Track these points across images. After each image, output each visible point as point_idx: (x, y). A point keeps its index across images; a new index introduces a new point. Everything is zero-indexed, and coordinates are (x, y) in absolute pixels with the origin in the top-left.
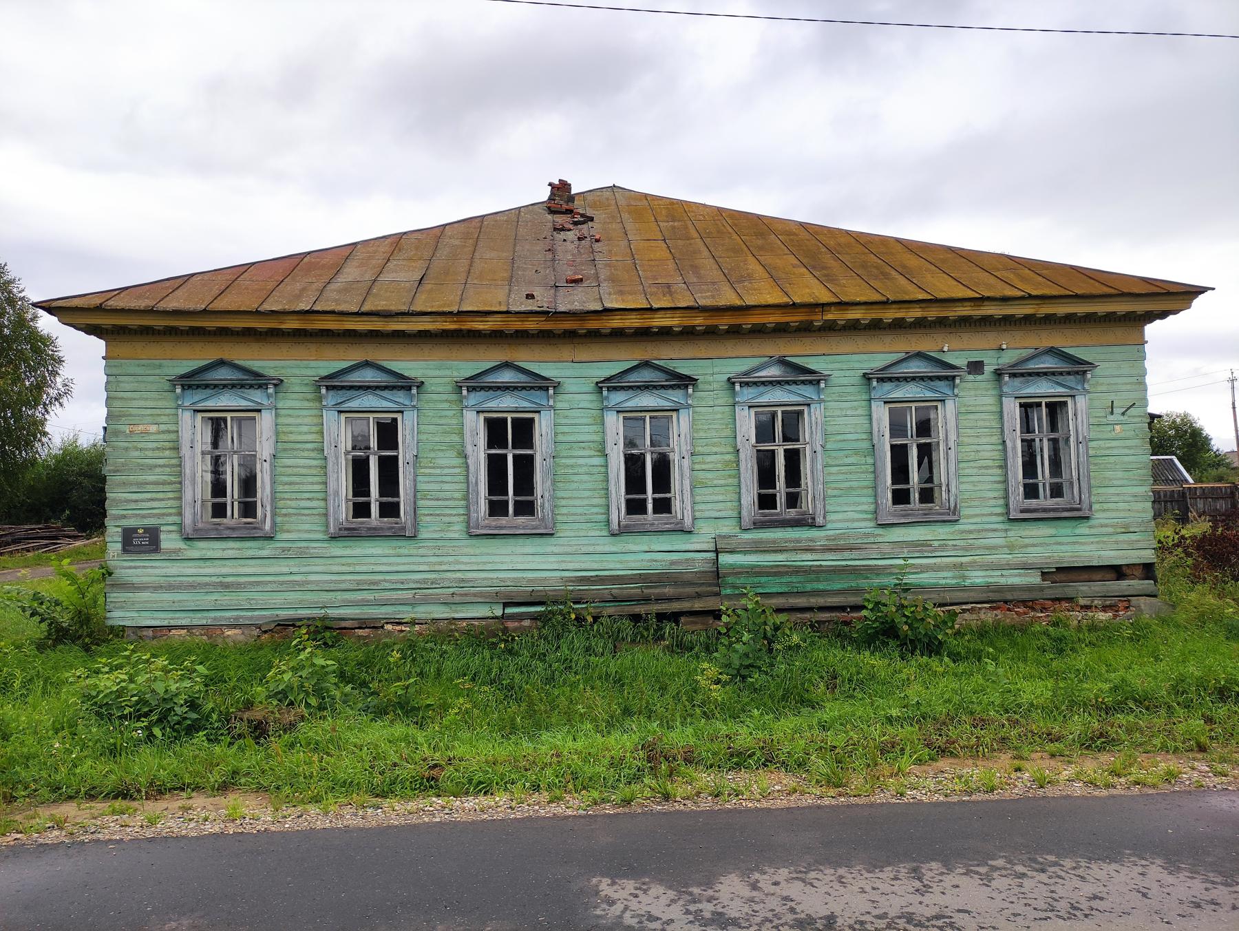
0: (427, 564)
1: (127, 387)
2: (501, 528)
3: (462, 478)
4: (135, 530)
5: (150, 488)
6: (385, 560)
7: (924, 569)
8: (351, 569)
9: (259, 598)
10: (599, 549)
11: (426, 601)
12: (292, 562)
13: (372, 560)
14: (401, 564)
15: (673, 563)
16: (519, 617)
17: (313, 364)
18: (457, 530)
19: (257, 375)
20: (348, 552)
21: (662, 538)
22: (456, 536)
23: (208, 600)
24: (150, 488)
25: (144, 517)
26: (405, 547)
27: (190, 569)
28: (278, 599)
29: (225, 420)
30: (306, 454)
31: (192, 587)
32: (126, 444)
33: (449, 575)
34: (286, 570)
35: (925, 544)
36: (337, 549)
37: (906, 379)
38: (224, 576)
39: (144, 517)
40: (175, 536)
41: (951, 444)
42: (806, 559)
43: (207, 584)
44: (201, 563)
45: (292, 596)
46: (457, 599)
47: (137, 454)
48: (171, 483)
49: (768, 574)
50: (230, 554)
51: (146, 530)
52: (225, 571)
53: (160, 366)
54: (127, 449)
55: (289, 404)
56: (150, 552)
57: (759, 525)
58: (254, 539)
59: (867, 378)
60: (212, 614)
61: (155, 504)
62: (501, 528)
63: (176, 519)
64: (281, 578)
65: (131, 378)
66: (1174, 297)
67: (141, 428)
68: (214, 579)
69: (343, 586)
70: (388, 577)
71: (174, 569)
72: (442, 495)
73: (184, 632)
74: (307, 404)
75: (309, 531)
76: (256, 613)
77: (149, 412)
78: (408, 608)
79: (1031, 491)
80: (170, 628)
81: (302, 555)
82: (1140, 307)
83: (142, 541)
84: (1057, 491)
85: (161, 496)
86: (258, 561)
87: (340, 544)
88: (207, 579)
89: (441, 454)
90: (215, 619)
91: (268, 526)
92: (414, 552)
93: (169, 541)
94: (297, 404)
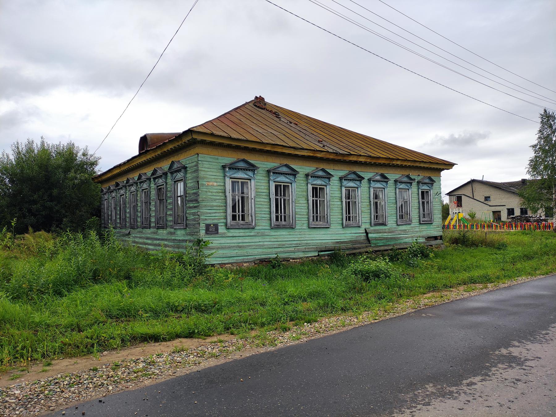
0: (297, 238)
1: (207, 166)
2: (317, 225)
3: (306, 208)
4: (209, 225)
5: (215, 208)
6: (286, 236)
7: (407, 238)
8: (277, 240)
9: (250, 251)
10: (340, 232)
11: (299, 251)
12: (260, 238)
13: (282, 237)
14: (290, 238)
15: (357, 237)
16: (324, 255)
17: (266, 163)
18: (305, 226)
19: (253, 165)
20: (276, 234)
21: (354, 229)
22: (305, 228)
23: (234, 252)
24: (215, 208)
25: (213, 219)
26: (292, 232)
27: (228, 241)
28: (256, 251)
29: (281, 185)
30: (264, 197)
31: (230, 247)
32: (206, 190)
33: (303, 242)
34: (258, 240)
35: (405, 231)
36: (273, 233)
37: (281, 174)
38: (239, 243)
39: (213, 219)
40: (224, 227)
41: (253, 197)
42: (385, 235)
43: (234, 246)
44: (231, 238)
45: (260, 250)
46: (307, 250)
47: (210, 194)
48: (222, 206)
49: (379, 240)
50: (241, 234)
51: (214, 225)
52: (240, 241)
53: (218, 159)
54: (206, 192)
55: (258, 178)
56: (215, 234)
57: (376, 225)
58: (248, 228)
59: (224, 167)
60: (235, 258)
61: (217, 215)
62: (317, 225)
63: (224, 221)
64: (256, 244)
65: (207, 163)
66: (449, 165)
67: (211, 183)
68: (236, 244)
69: (275, 246)
70: (287, 243)
71: (223, 241)
72: (301, 213)
73: (230, 265)
74: (264, 178)
75: (265, 226)
76: (249, 257)
77: (213, 177)
78: (293, 254)
79: (234, 217)
80: (225, 264)
81: (263, 235)
82: (441, 167)
83: (212, 229)
84: (243, 219)
85: (218, 211)
86: (250, 237)
87: (273, 231)
88: (233, 245)
89: (301, 199)
90: (236, 260)
91: (254, 224)
92: (294, 233)
93: (222, 229)
94: (261, 178)
